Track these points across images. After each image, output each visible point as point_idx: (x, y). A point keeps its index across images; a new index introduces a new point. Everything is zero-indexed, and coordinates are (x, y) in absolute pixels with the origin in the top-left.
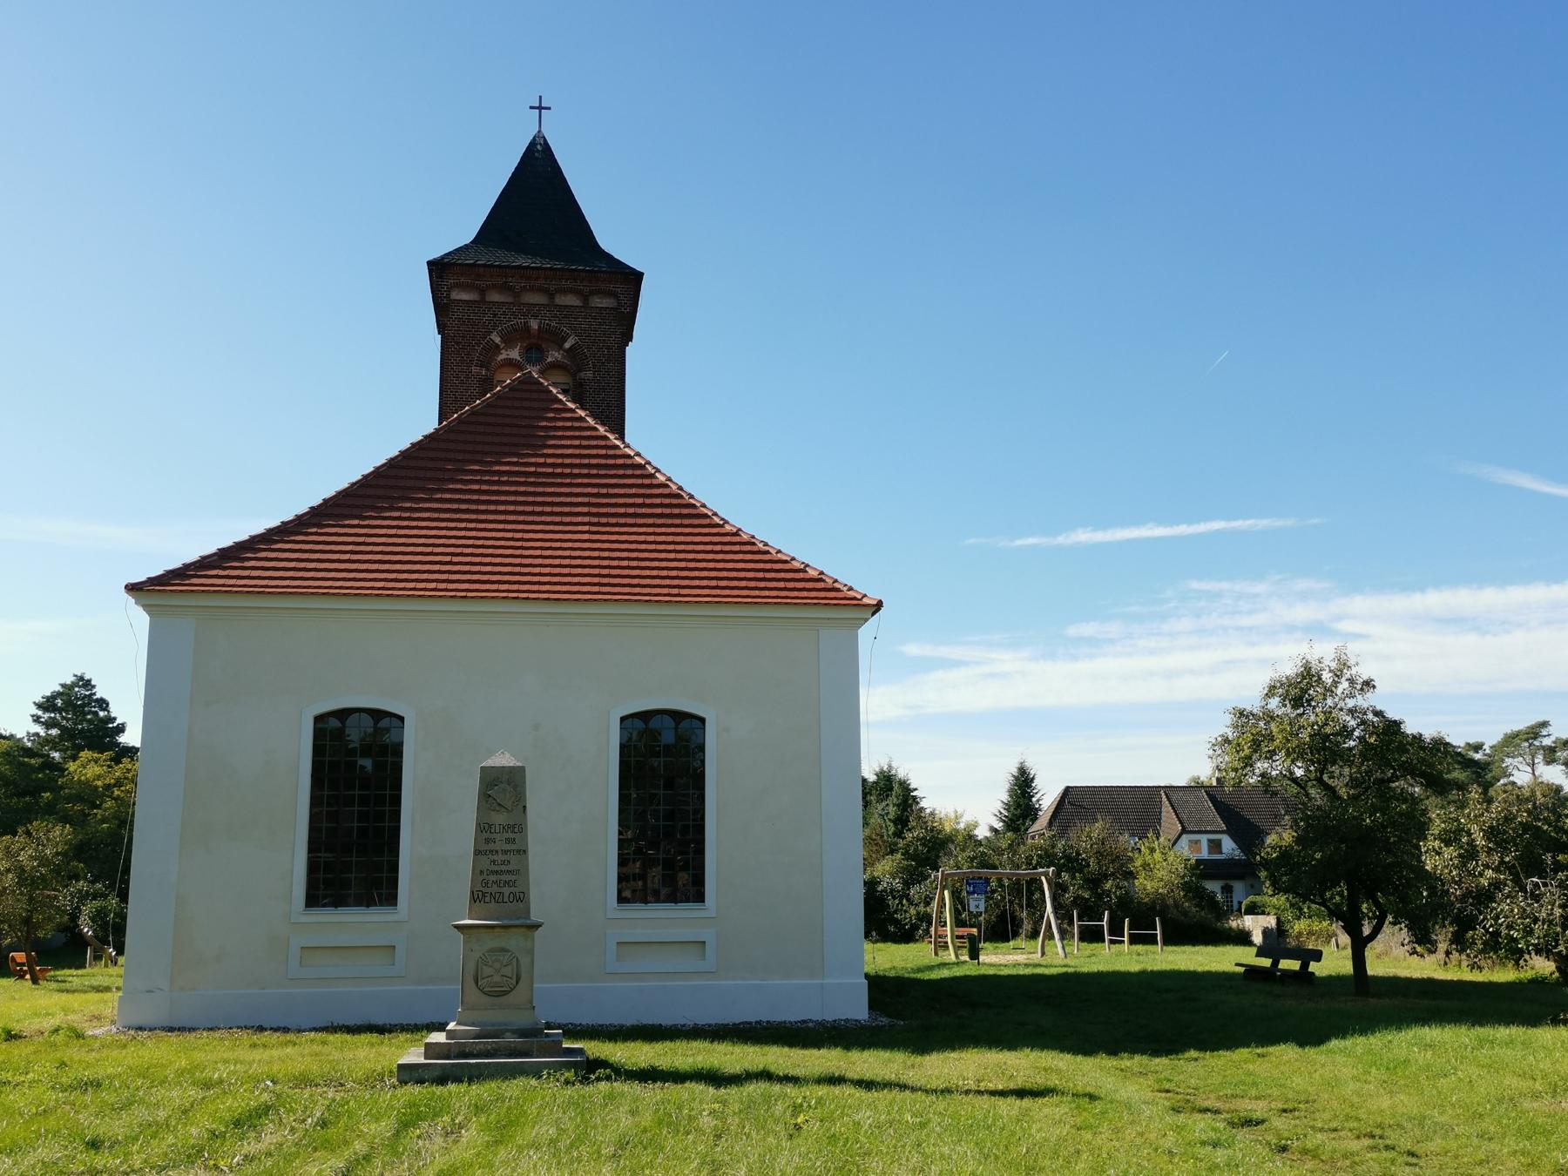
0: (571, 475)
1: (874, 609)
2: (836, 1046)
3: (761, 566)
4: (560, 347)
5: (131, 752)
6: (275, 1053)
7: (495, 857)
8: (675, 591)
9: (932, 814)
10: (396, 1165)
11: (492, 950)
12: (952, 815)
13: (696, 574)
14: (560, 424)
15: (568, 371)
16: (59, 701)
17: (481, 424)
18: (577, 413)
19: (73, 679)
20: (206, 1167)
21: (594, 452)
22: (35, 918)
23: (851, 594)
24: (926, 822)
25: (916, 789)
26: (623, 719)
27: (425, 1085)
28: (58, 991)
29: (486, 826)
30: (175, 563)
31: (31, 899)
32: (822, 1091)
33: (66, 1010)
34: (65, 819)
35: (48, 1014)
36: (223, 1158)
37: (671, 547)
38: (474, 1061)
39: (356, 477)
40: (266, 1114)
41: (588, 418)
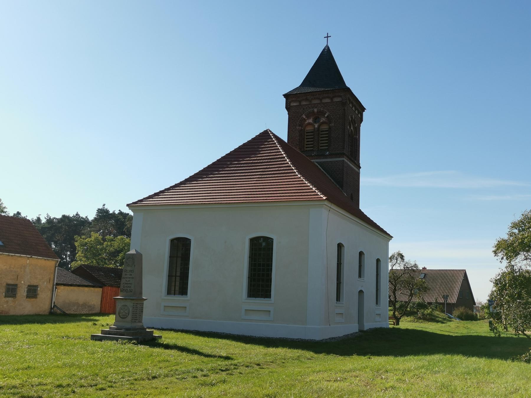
11: (123, 306)
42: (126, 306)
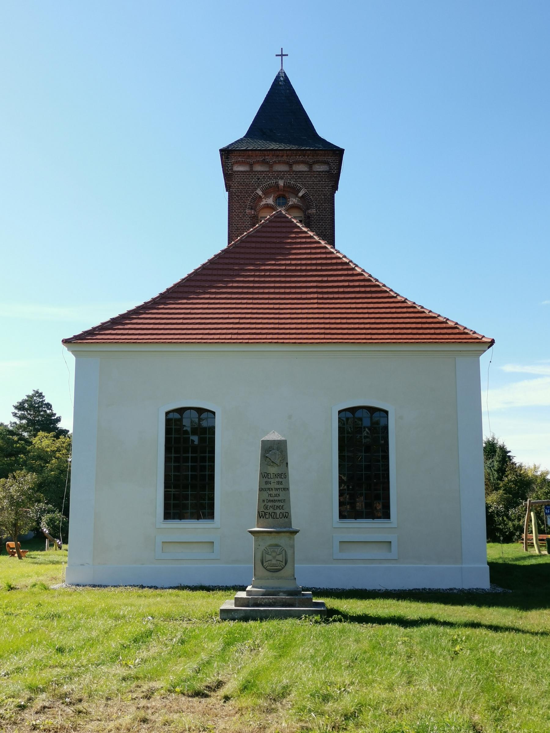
0: (306, 270)
1: (489, 344)
2: (473, 604)
3: (420, 320)
4: (297, 195)
5: (64, 432)
6: (151, 600)
7: (271, 492)
8: (369, 336)
9: (520, 466)
10: (225, 668)
11: (270, 546)
12: (532, 467)
13: (381, 326)
14: (299, 240)
15: (301, 209)
16: (26, 404)
17: (253, 242)
18: (308, 233)
19: (33, 392)
20: (121, 665)
21: (319, 256)
22: (20, 523)
23: (475, 336)
24: (516, 471)
25: (510, 452)
26: (340, 412)
27: (236, 621)
28: (33, 563)
29: (266, 474)
30: (88, 328)
31: (16, 513)
32: (468, 631)
33: (38, 574)
34: (31, 469)
35: (28, 576)
36: (130, 660)
37: (366, 311)
38: (263, 609)
39: (185, 275)
40: (151, 635)
41: (315, 237)
42: (279, 546)
